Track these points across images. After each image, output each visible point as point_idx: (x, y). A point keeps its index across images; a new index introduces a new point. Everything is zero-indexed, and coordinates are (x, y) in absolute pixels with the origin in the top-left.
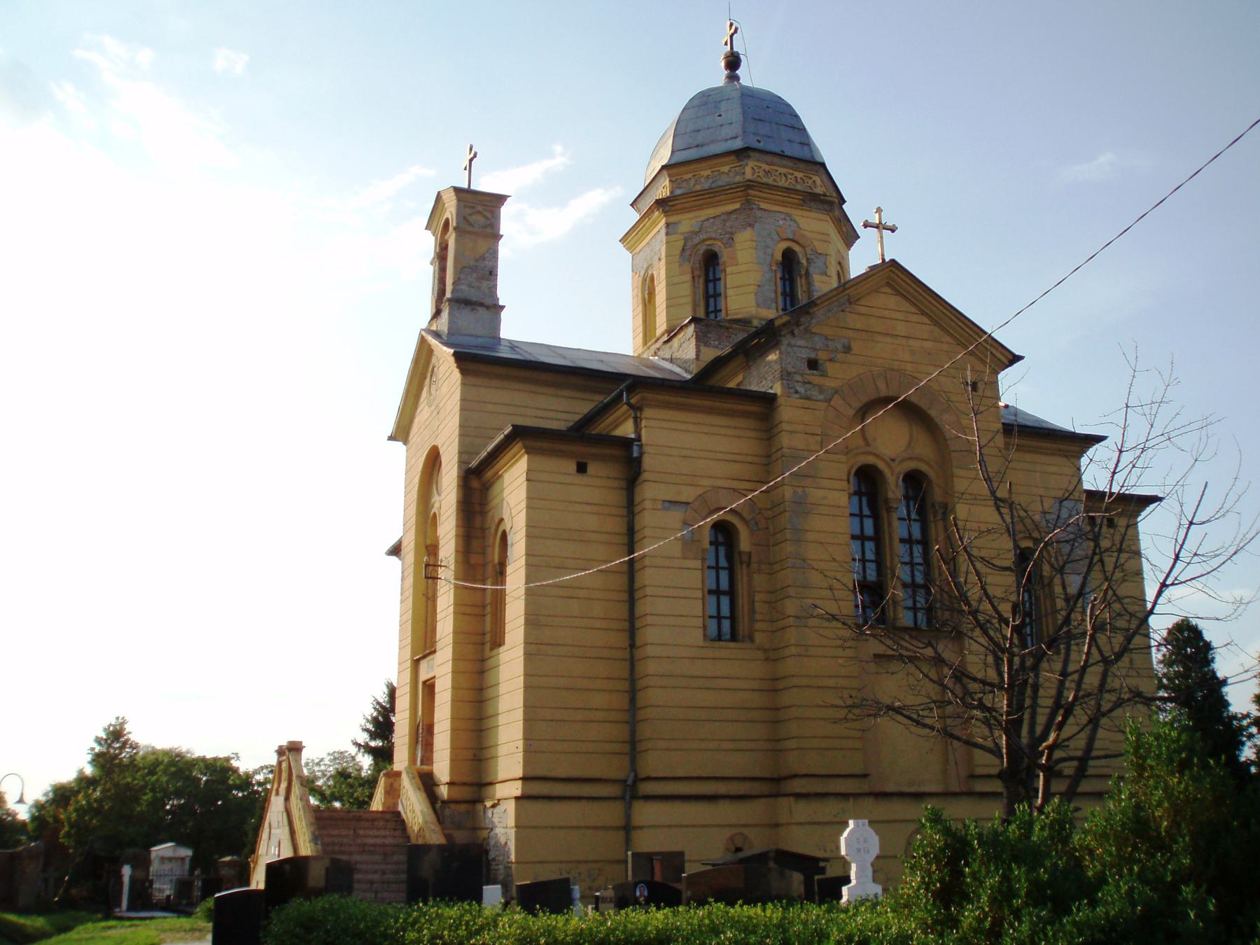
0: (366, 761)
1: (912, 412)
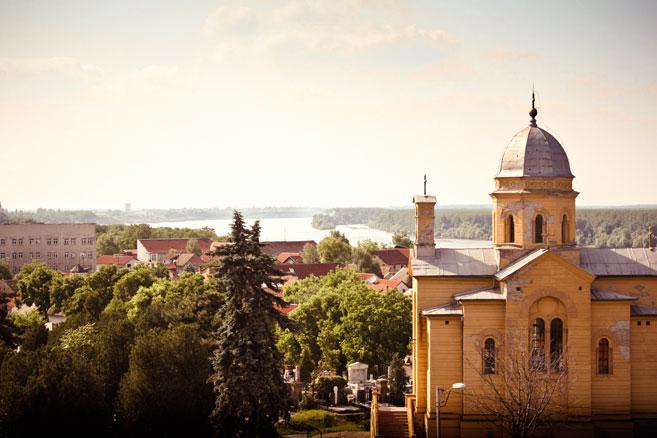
1: (556, 300)
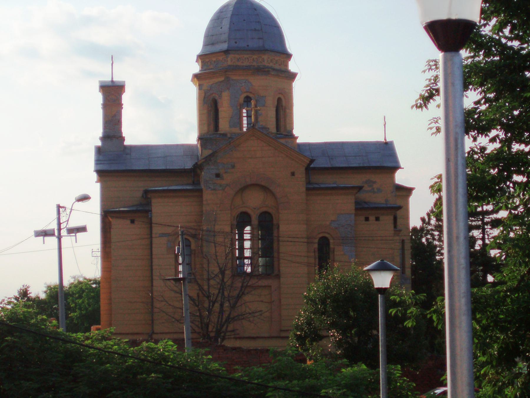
0: (57, 324)
1: (265, 189)
